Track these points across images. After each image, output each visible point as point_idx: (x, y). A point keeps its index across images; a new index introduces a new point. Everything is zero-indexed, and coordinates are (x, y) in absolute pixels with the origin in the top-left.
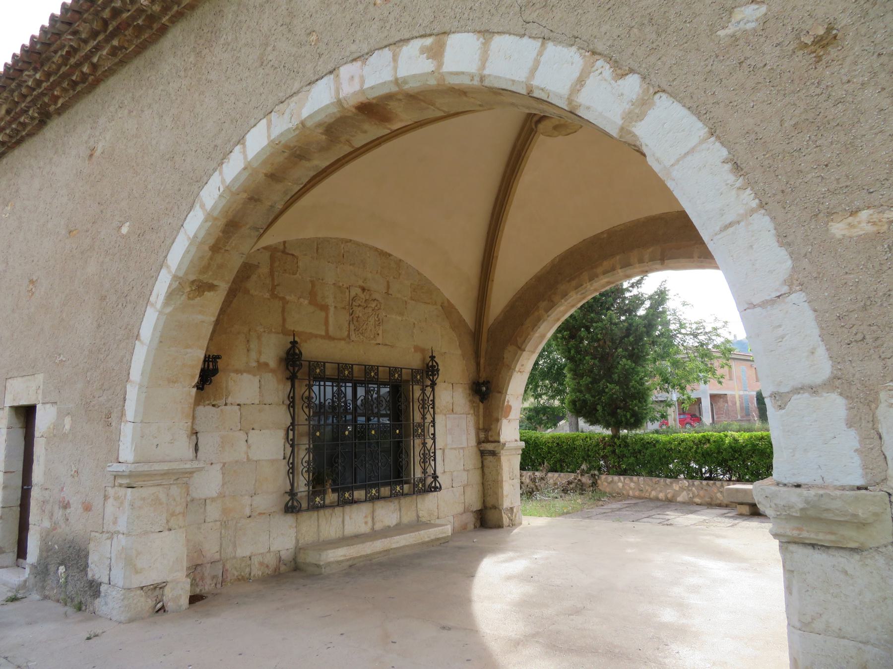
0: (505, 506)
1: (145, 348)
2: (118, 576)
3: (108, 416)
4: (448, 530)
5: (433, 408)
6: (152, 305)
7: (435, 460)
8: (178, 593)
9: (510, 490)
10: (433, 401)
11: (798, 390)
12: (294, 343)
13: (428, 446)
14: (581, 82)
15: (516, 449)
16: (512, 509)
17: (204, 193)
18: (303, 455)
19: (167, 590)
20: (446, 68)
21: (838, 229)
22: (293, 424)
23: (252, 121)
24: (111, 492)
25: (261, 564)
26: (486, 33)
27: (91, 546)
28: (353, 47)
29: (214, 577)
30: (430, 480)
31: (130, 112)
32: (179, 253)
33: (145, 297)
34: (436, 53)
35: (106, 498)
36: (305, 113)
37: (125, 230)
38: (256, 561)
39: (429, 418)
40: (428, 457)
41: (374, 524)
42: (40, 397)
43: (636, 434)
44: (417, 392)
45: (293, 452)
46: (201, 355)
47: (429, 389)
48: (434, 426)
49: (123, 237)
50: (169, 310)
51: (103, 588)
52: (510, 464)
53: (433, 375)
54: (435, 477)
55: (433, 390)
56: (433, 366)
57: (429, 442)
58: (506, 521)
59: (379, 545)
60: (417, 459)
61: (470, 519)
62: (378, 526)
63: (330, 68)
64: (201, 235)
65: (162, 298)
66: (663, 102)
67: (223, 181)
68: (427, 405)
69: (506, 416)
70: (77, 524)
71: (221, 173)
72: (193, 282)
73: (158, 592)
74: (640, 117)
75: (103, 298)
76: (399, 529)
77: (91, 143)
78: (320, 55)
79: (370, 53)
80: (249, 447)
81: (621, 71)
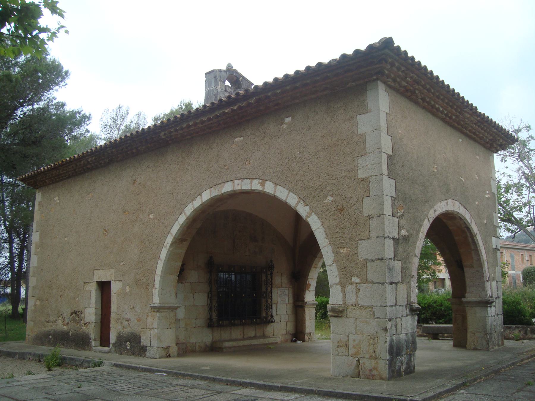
0: (306, 332)
1: (163, 262)
2: (155, 343)
3: (147, 286)
5: (271, 284)
7: (272, 309)
8: (174, 350)
10: (271, 281)
11: (334, 285)
12: (211, 257)
13: (269, 302)
14: (297, 204)
15: (313, 305)
16: (310, 333)
18: (214, 303)
19: (170, 349)
20: (265, 190)
21: (342, 251)
22: (211, 291)
23: (204, 189)
24: (150, 314)
25: (199, 346)
27: (142, 334)
28: (239, 175)
29: (183, 349)
30: (269, 318)
31: (153, 170)
32: (175, 229)
33: (162, 244)
34: (263, 185)
35: (147, 316)
36: (223, 191)
37: (151, 216)
38: (197, 345)
39: (269, 290)
40: (269, 307)
41: (244, 335)
42: (113, 278)
44: (264, 278)
45: (211, 302)
46: (180, 264)
47: (269, 276)
48: (271, 293)
49: (151, 219)
50: (171, 249)
53: (271, 269)
54: (272, 316)
55: (272, 277)
56: (271, 265)
57: (269, 300)
58: (306, 338)
59: (246, 343)
60: (264, 308)
61: (289, 337)
62: (246, 336)
63: (231, 179)
64: (185, 224)
65: (169, 245)
67: (193, 207)
68: (270, 283)
70: (134, 327)
71: (192, 204)
72: (180, 239)
73: (167, 350)
74: (309, 217)
75: (142, 242)
76: (255, 337)
77: (134, 178)
78: (228, 174)
79: (244, 179)
80: (194, 300)
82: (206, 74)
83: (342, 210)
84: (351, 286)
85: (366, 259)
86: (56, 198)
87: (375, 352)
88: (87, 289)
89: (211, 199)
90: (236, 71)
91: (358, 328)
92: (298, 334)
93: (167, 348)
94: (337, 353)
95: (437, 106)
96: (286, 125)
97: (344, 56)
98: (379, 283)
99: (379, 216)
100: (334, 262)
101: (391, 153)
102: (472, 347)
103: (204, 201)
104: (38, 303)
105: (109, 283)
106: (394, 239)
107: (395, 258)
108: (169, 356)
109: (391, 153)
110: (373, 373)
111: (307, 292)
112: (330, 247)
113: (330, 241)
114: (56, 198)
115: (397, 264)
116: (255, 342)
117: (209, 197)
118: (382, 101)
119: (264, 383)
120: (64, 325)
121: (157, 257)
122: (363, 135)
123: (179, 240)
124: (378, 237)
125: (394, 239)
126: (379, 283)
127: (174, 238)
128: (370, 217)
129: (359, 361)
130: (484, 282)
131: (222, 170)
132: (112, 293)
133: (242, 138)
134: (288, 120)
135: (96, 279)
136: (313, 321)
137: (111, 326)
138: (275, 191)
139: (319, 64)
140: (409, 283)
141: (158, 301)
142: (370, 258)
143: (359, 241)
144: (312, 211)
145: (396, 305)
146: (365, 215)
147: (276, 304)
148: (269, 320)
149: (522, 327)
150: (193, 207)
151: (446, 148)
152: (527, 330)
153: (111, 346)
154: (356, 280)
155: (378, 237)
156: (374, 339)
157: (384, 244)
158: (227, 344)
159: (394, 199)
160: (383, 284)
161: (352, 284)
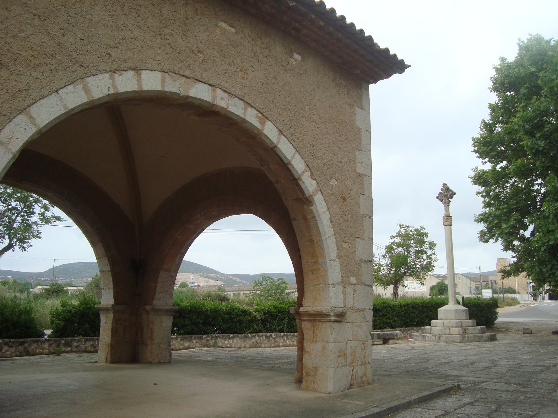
34: (263, 123)
63: (211, 83)
79: (235, 96)
102: (157, 360)
110: (363, 380)
112: (334, 238)
131: (192, 55)
133: (233, 30)
143: (357, 239)
149: (54, 340)
152: (60, 343)
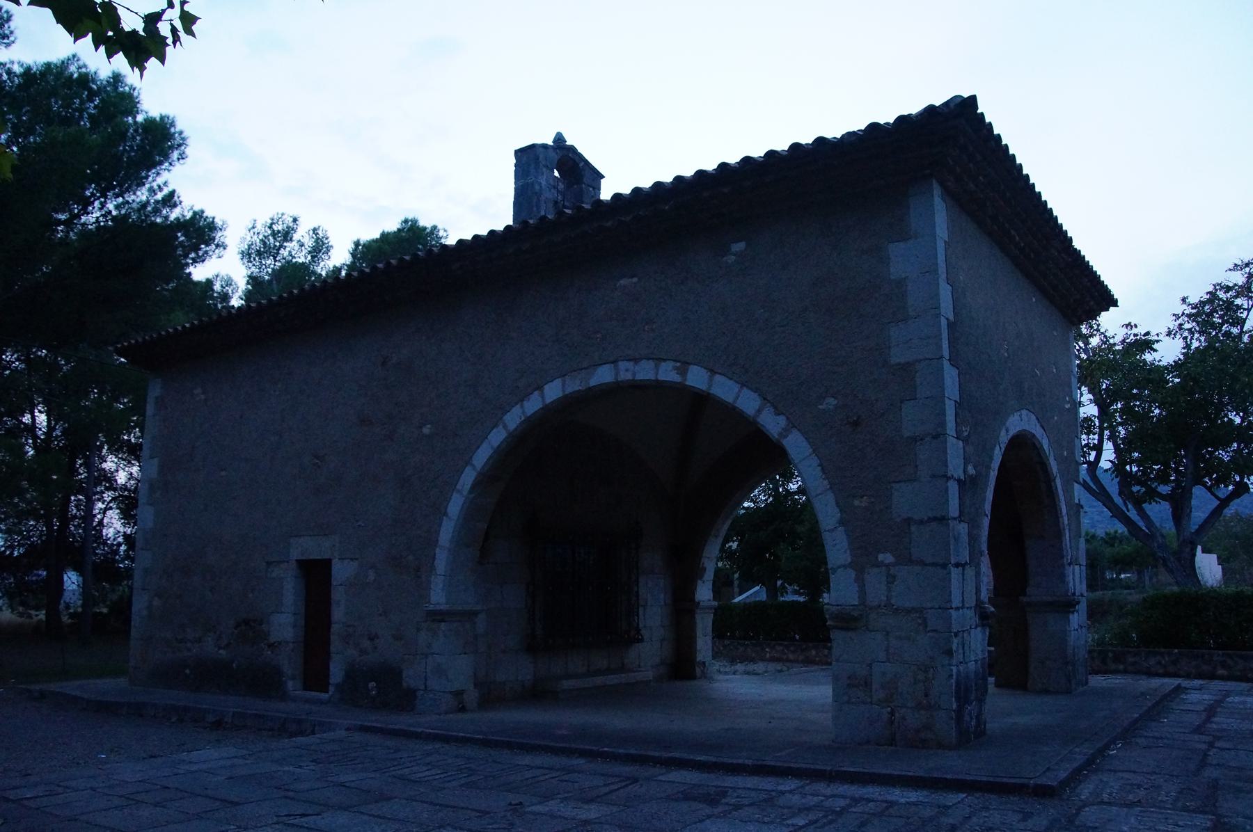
1: (453, 524)
4: (650, 675)
6: (459, 491)
8: (472, 696)
9: (704, 644)
14: (759, 411)
15: (710, 608)
17: (507, 417)
21: (856, 503)
26: (713, 372)
34: (683, 372)
36: (593, 382)
37: (426, 430)
43: (1244, 703)
51: (419, 693)
52: (704, 625)
54: (638, 631)
58: (698, 671)
59: (599, 680)
66: (795, 431)
69: (701, 578)
71: (522, 407)
74: (786, 437)
76: (608, 671)
81: (778, 413)
82: (516, 152)
83: (856, 424)
84: (876, 570)
85: (909, 519)
86: (198, 391)
87: (926, 695)
88: (274, 575)
89: (565, 397)
90: (572, 149)
91: (891, 651)
92: (682, 666)
93: (458, 694)
94: (846, 698)
95: (1013, 232)
96: (733, 258)
97: (874, 127)
98: (934, 564)
99: (935, 437)
100: (842, 522)
101: (952, 318)
103: (548, 401)
104: (156, 602)
105: (326, 564)
106: (959, 481)
107: (960, 519)
108: (463, 709)
109: (952, 318)
111: (699, 582)
113: (830, 483)
114: (198, 391)
115: (963, 528)
116: (613, 679)
117: (561, 395)
118: (937, 217)
119: (713, 759)
120: (220, 648)
121: (439, 511)
122: (901, 283)
123: (485, 480)
124: (933, 476)
125: (959, 481)
126: (934, 564)
127: (480, 474)
128: (914, 439)
129: (892, 713)
130: (1063, 565)
132: (334, 583)
133: (635, 280)
134: (739, 247)
135: (295, 554)
136: (709, 639)
137: (332, 649)
138: (710, 386)
139: (820, 141)
140: (978, 566)
141: (443, 600)
142: (916, 517)
144: (791, 425)
145: (962, 608)
146: (907, 434)
147: (645, 607)
148: (634, 637)
150: (524, 412)
151: (1010, 309)
153: (332, 689)
154: (887, 558)
155: (933, 476)
156: (926, 671)
157: (947, 490)
158: (567, 684)
159: (959, 405)
160: (944, 566)
161: (879, 565)
